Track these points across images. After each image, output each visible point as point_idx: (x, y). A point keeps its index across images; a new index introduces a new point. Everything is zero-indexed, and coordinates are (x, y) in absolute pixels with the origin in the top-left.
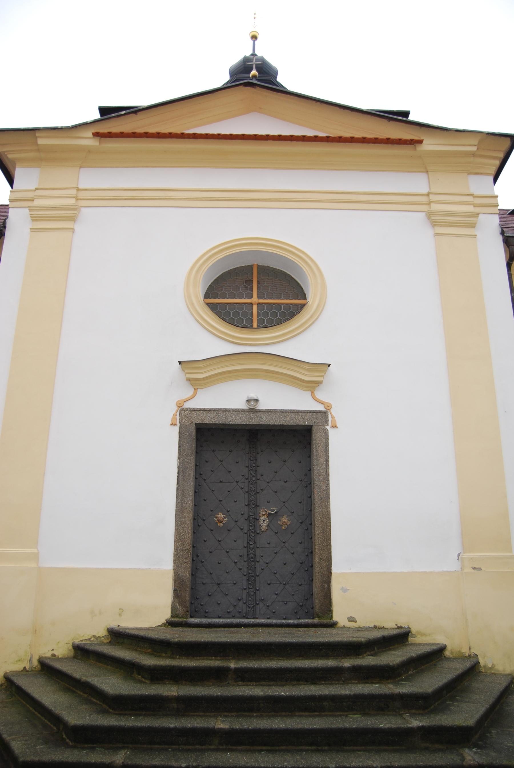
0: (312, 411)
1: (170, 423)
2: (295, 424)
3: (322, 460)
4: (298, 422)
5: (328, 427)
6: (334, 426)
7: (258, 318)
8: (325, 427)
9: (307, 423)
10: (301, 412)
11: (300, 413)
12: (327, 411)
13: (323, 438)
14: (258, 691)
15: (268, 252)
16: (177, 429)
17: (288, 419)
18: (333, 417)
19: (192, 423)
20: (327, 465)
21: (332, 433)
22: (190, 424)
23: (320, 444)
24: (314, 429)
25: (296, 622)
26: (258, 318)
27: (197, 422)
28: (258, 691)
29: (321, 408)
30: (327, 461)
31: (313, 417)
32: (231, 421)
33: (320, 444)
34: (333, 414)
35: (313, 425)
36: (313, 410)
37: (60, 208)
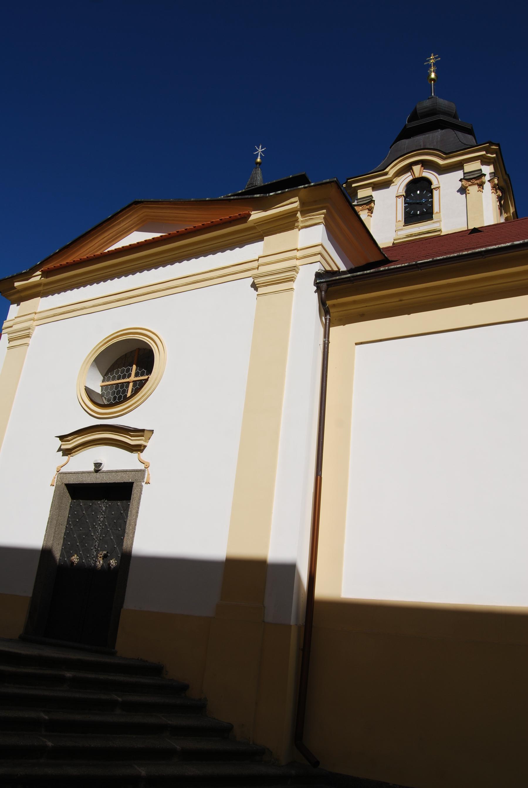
0: (135, 470)
1: (50, 484)
2: (123, 482)
3: (134, 511)
4: (125, 480)
5: (143, 484)
6: (148, 483)
7: (146, 377)
8: (141, 483)
9: (130, 480)
10: (128, 471)
11: (128, 472)
12: (145, 470)
13: (139, 493)
14: (91, 676)
15: (427, 123)
16: (54, 488)
17: (119, 478)
18: (149, 475)
19: (63, 483)
20: (137, 516)
21: (145, 486)
22: (62, 484)
23: (136, 498)
24: (135, 485)
25: (510, 187)
26: (146, 377)
27: (65, 483)
28: (91, 676)
29: (141, 467)
30: (137, 512)
31: (135, 475)
32: (85, 481)
33: (136, 498)
34: (150, 473)
35: (134, 482)
36: (136, 469)
37: (170, 257)
